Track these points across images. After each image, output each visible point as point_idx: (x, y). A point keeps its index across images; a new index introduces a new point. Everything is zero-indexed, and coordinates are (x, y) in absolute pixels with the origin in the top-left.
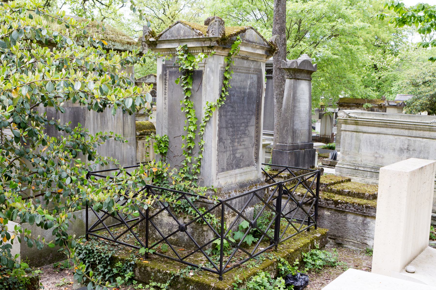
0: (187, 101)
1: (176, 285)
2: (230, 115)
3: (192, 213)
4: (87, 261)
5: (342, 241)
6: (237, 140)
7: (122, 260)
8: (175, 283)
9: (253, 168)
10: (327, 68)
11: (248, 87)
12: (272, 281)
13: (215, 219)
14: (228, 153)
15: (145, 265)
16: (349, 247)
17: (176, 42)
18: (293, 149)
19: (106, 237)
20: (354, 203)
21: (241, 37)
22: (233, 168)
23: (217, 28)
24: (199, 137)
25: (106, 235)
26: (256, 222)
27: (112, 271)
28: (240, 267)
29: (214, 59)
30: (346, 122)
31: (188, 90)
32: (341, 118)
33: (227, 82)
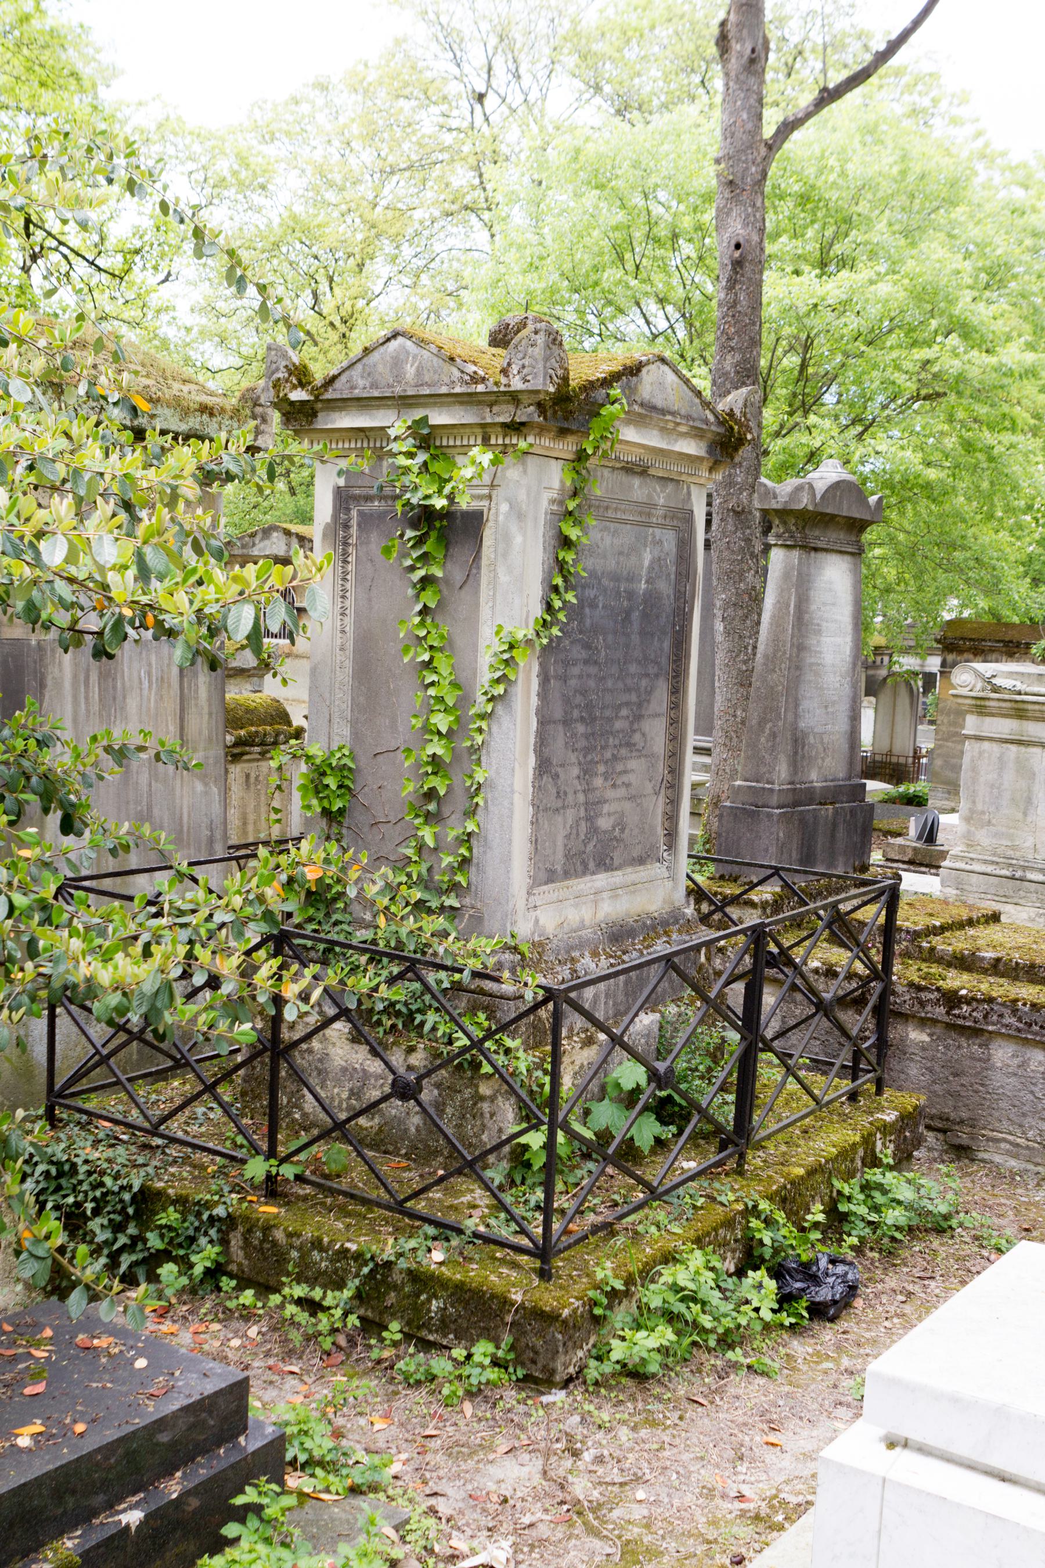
0: (422, 623)
1: (381, 1297)
2: (580, 677)
3: (440, 1033)
4: (49, 1205)
5: (973, 1137)
6: (601, 769)
7: (181, 1202)
8: (376, 1289)
9: (657, 870)
10: (902, 513)
11: (644, 572)
12: (730, 1283)
13: (521, 1054)
14: (570, 814)
15: (267, 1220)
16: (997, 1159)
17: (388, 407)
18: (796, 804)
19: (120, 1117)
20: (1016, 1000)
21: (623, 392)
22: (585, 871)
23: (540, 358)
24: (466, 755)
25: (120, 1108)
26: (670, 1070)
27: (145, 1241)
28: (613, 1234)
29: (525, 472)
30: (980, 707)
31: (426, 581)
32: (964, 692)
33: (569, 557)
